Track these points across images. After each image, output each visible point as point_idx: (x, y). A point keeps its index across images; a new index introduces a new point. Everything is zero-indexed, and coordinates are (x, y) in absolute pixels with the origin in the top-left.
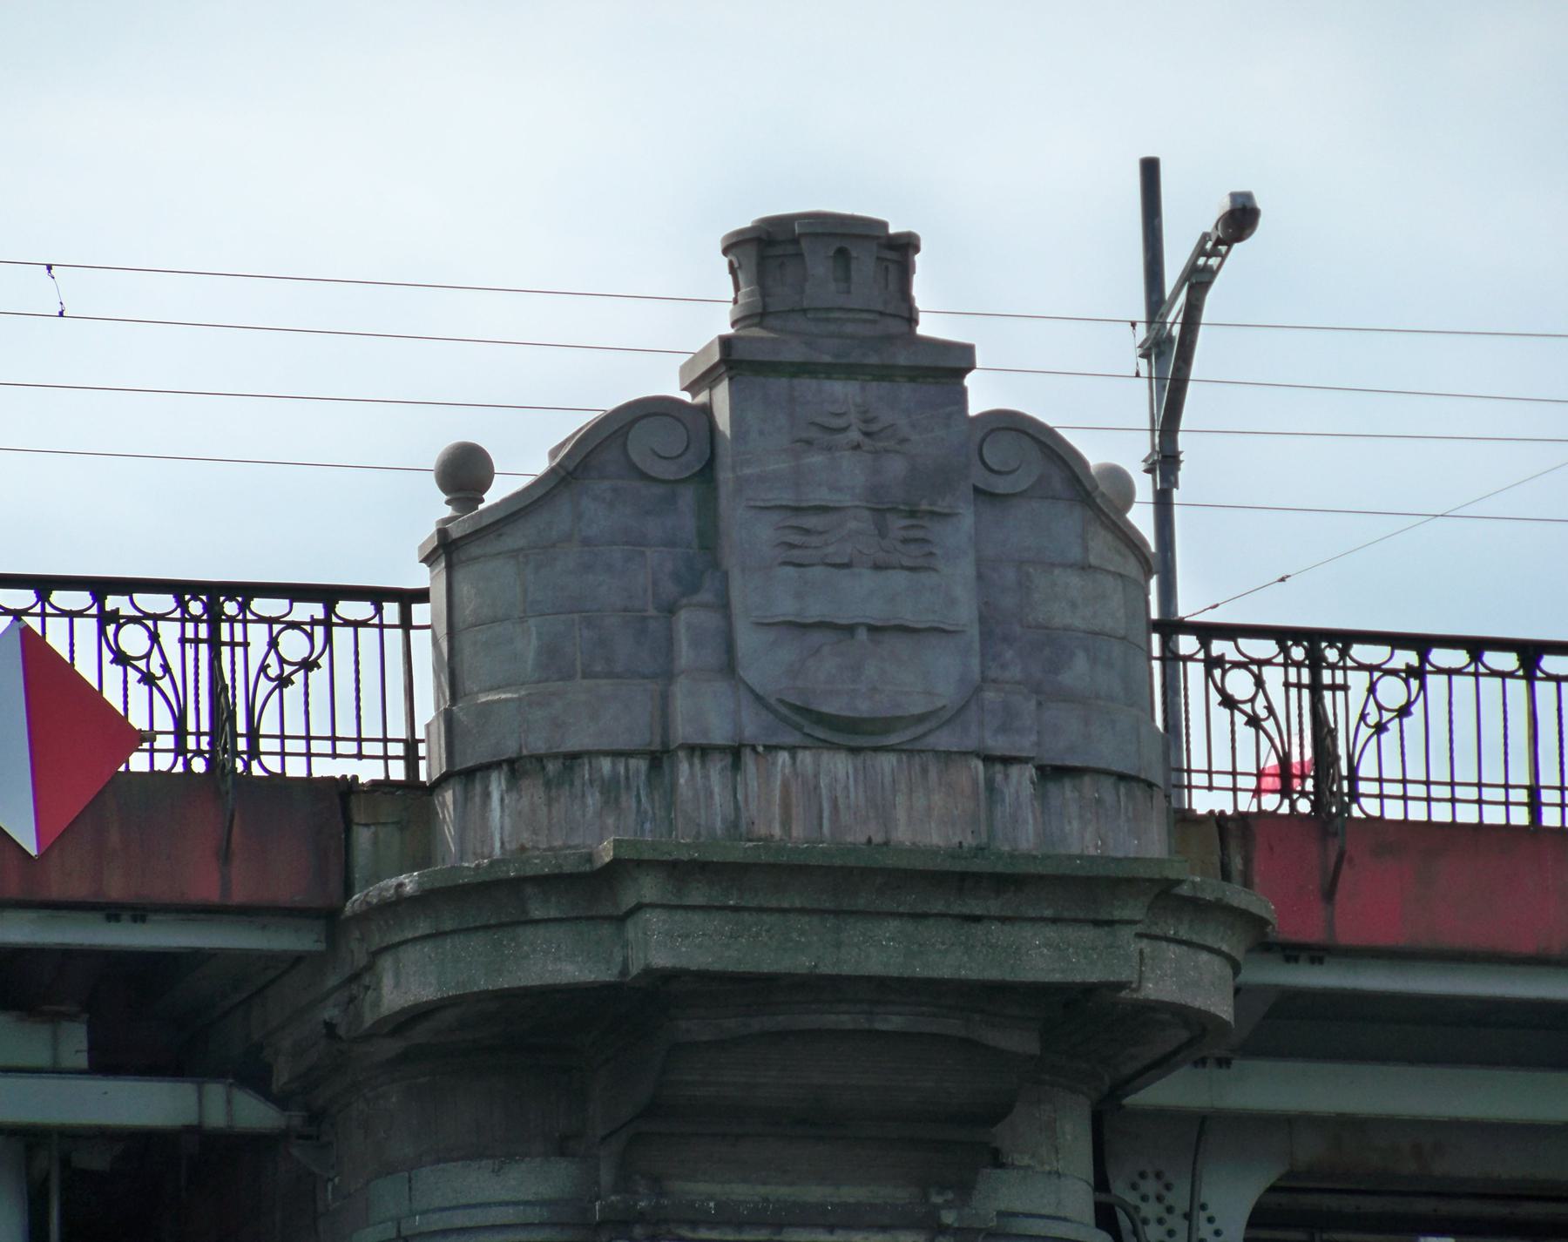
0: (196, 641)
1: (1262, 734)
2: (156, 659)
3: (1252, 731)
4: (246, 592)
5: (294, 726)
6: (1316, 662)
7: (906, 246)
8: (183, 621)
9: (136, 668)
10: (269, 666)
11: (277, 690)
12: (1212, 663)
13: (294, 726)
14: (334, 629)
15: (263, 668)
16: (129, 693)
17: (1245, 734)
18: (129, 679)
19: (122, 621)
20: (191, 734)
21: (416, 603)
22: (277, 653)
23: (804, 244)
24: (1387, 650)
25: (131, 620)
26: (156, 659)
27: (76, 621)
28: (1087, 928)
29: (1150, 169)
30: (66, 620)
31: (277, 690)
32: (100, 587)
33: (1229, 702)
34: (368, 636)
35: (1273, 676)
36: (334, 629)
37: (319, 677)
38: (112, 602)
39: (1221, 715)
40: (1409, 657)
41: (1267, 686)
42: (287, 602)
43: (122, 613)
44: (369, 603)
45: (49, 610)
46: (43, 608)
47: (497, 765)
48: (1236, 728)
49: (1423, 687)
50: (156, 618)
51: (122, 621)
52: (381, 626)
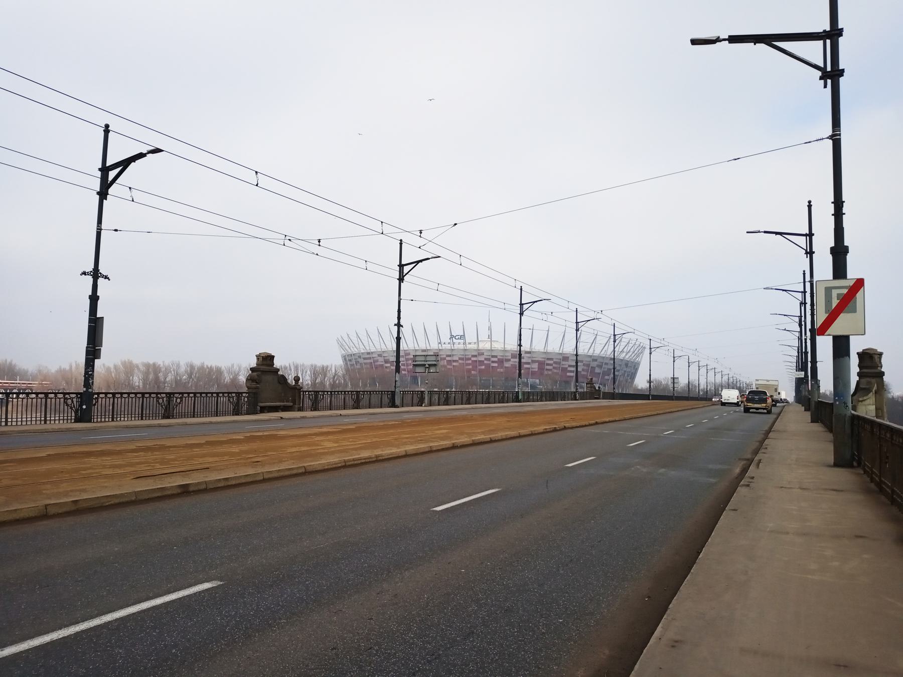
2: (73, 405)
4: (174, 394)
13: (178, 412)
24: (178, 395)
25: (69, 399)
26: (73, 405)
29: (810, 202)
39: (66, 407)
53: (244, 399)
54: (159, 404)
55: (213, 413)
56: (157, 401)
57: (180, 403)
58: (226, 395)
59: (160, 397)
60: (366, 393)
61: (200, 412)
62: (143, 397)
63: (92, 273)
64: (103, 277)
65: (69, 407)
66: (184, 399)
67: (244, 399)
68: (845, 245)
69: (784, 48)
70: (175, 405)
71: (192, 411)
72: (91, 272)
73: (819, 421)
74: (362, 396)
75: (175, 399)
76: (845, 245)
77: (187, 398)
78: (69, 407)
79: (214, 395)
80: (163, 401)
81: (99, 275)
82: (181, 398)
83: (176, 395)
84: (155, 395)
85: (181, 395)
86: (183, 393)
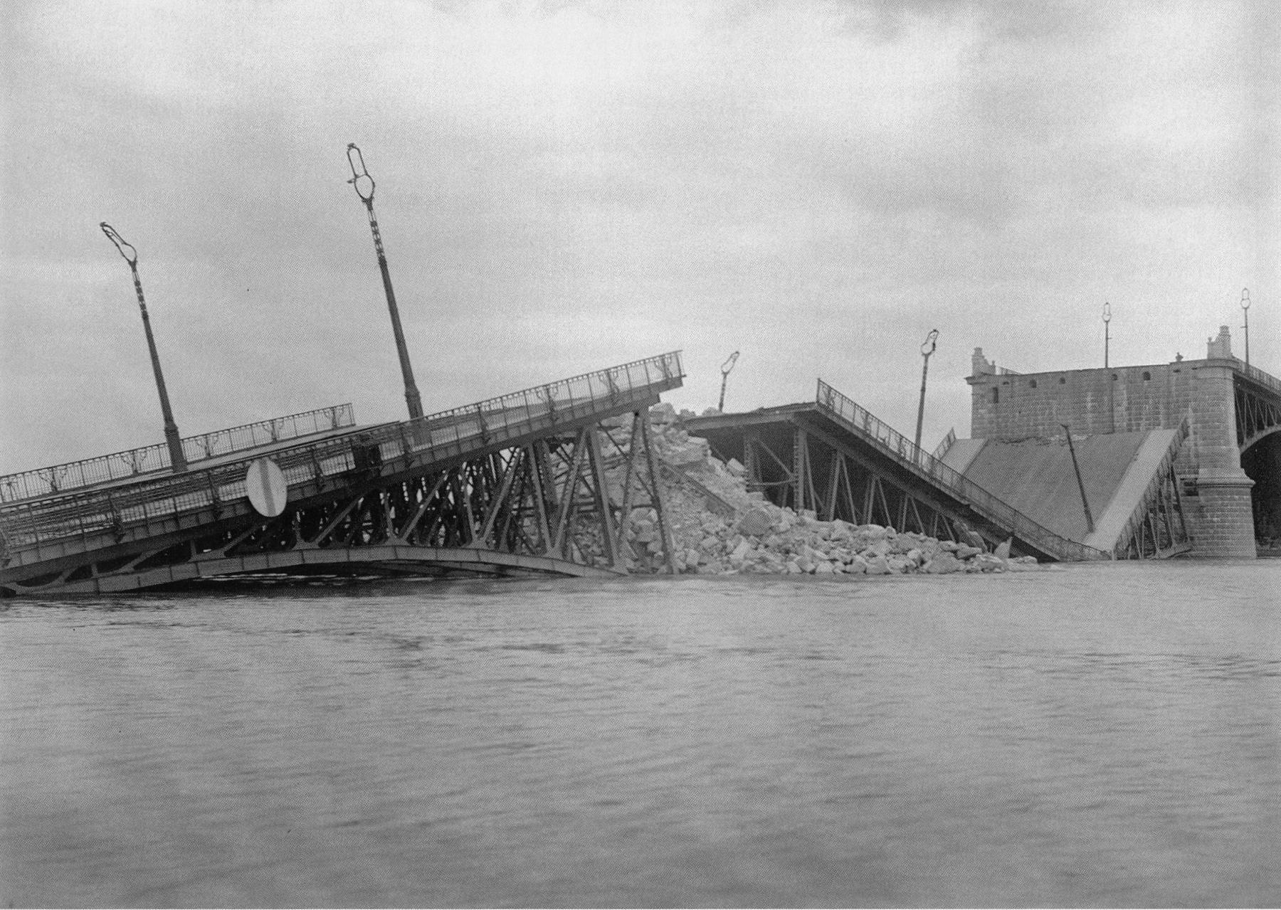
4: (136, 450)
12: (40, 474)
37: (67, 476)
40: (216, 434)
75: (59, 471)
83: (212, 435)
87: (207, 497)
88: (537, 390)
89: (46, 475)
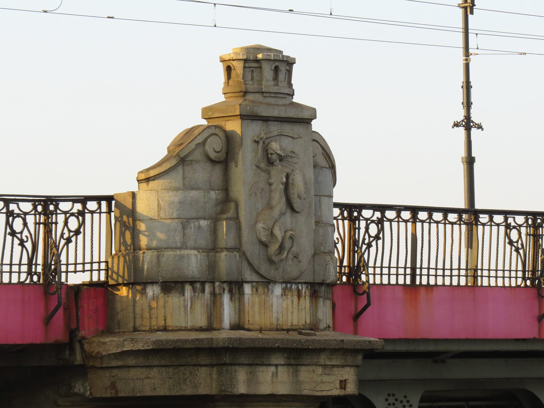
0: (39, 224)
1: (24, 249)
3: (20, 247)
4: (361, 207)
5: (72, 260)
6: (46, 213)
7: (289, 63)
8: (35, 215)
9: (514, 246)
10: (64, 233)
11: (66, 246)
14: (361, 221)
15: (62, 234)
16: (378, 255)
17: (514, 254)
18: (14, 242)
19: (15, 215)
20: (418, 275)
21: (88, 201)
22: (68, 228)
23: (262, 62)
24: (371, 212)
25: (18, 215)
26: (520, 242)
27: (454, 226)
28: (254, 367)
30: (389, 223)
31: (66, 246)
32: (506, 213)
33: (511, 243)
34: (456, 227)
35: (30, 219)
36: (361, 221)
38: (13, 207)
39: (508, 247)
40: (78, 207)
41: (28, 225)
42: (372, 211)
43: (15, 212)
44: (3, 202)
45: (432, 221)
46: (430, 221)
47: (199, 282)
48: (14, 246)
49: (82, 224)
50: (26, 214)
51: (15, 215)
52: (100, 213)
53: (367, 228)
54: (511, 243)
55: (401, 271)
56: (507, 235)
57: (377, 238)
58: (499, 219)
59: (17, 211)
60: (423, 215)
61: (382, 267)
62: (414, 219)
63: (464, 123)
64: (475, 127)
65: (513, 248)
66: (387, 225)
67: (367, 228)
68: (473, 156)
69: (311, 106)
70: (363, 242)
71: (409, 265)
72: (463, 121)
73: (108, 284)
74: (73, 223)
75: (61, 218)
76: (473, 156)
77: (441, 226)
78: (513, 248)
79: (464, 216)
80: (25, 224)
81: (472, 124)
82: (380, 222)
83: (64, 206)
84: (456, 215)
85: (78, 207)
86: (382, 208)
87: (524, 271)
88: (13, 207)
89: (520, 233)
